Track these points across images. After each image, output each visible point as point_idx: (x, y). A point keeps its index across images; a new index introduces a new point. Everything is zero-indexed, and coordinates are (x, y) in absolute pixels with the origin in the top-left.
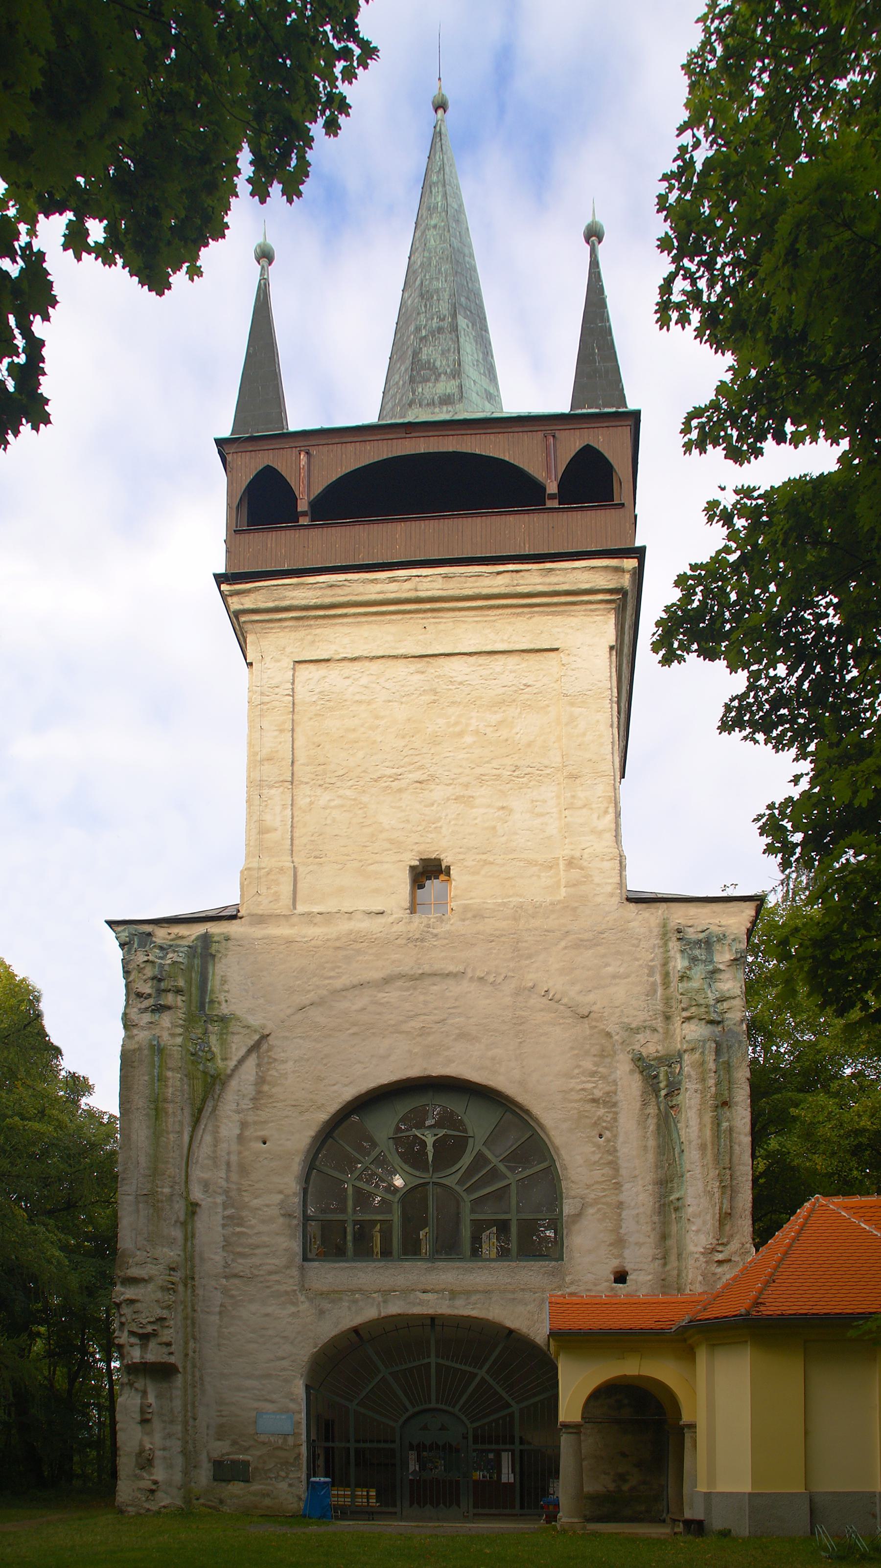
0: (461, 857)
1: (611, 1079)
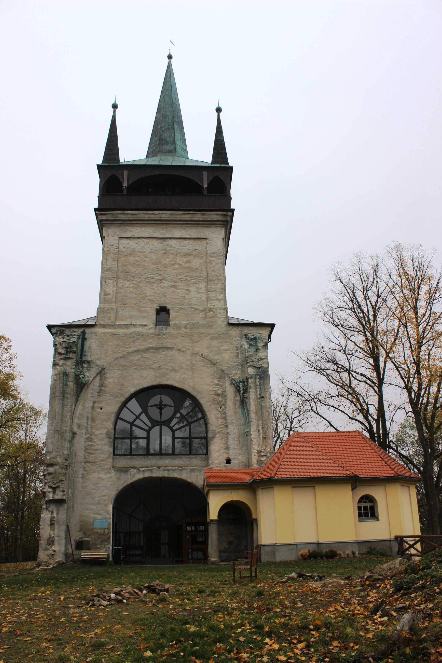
0: (173, 306)
1: (224, 386)
